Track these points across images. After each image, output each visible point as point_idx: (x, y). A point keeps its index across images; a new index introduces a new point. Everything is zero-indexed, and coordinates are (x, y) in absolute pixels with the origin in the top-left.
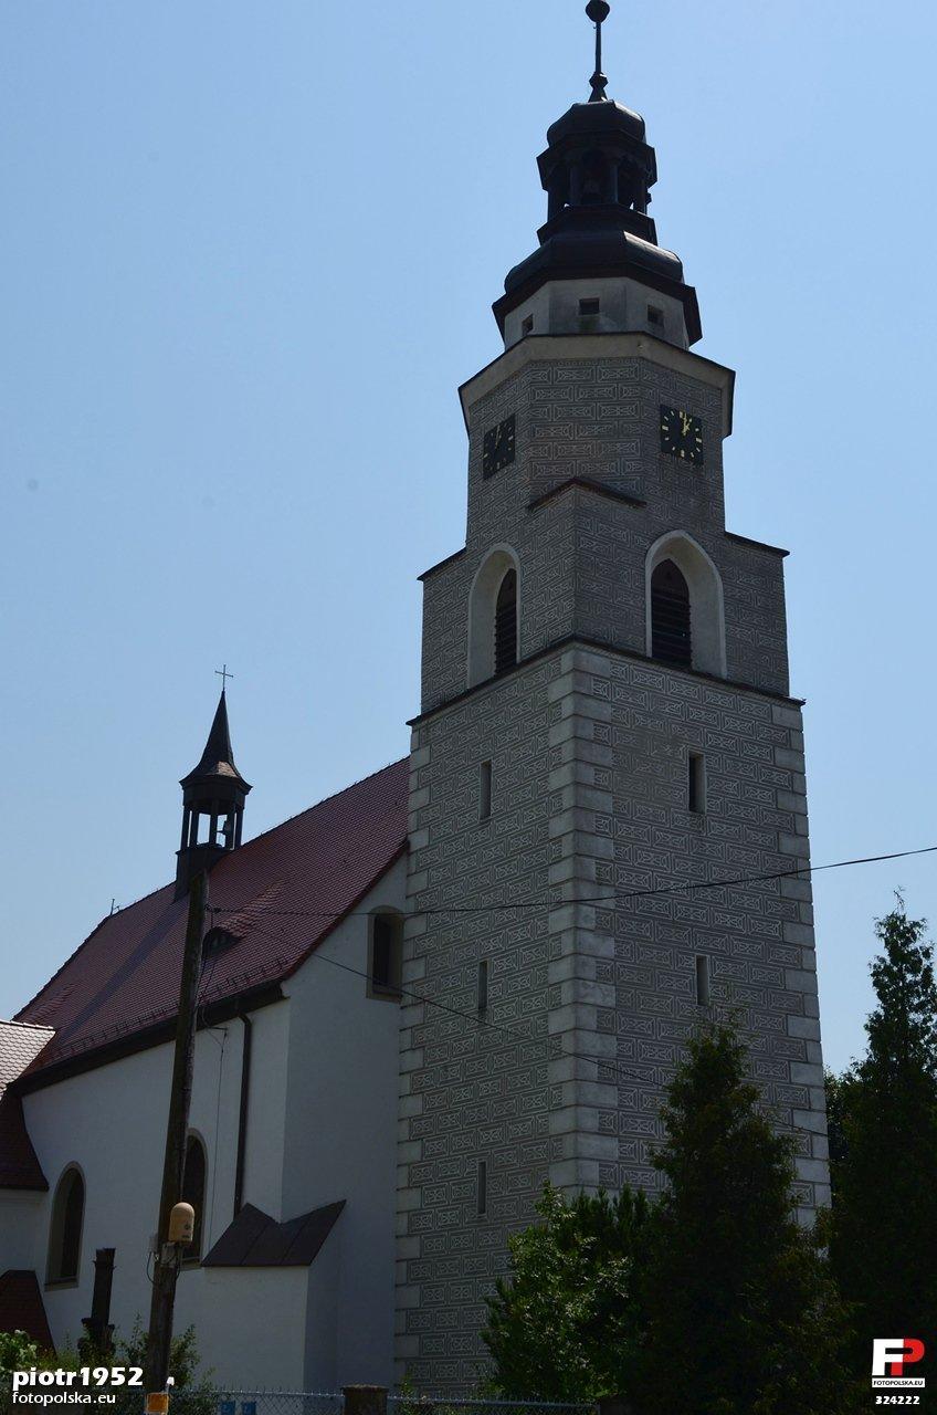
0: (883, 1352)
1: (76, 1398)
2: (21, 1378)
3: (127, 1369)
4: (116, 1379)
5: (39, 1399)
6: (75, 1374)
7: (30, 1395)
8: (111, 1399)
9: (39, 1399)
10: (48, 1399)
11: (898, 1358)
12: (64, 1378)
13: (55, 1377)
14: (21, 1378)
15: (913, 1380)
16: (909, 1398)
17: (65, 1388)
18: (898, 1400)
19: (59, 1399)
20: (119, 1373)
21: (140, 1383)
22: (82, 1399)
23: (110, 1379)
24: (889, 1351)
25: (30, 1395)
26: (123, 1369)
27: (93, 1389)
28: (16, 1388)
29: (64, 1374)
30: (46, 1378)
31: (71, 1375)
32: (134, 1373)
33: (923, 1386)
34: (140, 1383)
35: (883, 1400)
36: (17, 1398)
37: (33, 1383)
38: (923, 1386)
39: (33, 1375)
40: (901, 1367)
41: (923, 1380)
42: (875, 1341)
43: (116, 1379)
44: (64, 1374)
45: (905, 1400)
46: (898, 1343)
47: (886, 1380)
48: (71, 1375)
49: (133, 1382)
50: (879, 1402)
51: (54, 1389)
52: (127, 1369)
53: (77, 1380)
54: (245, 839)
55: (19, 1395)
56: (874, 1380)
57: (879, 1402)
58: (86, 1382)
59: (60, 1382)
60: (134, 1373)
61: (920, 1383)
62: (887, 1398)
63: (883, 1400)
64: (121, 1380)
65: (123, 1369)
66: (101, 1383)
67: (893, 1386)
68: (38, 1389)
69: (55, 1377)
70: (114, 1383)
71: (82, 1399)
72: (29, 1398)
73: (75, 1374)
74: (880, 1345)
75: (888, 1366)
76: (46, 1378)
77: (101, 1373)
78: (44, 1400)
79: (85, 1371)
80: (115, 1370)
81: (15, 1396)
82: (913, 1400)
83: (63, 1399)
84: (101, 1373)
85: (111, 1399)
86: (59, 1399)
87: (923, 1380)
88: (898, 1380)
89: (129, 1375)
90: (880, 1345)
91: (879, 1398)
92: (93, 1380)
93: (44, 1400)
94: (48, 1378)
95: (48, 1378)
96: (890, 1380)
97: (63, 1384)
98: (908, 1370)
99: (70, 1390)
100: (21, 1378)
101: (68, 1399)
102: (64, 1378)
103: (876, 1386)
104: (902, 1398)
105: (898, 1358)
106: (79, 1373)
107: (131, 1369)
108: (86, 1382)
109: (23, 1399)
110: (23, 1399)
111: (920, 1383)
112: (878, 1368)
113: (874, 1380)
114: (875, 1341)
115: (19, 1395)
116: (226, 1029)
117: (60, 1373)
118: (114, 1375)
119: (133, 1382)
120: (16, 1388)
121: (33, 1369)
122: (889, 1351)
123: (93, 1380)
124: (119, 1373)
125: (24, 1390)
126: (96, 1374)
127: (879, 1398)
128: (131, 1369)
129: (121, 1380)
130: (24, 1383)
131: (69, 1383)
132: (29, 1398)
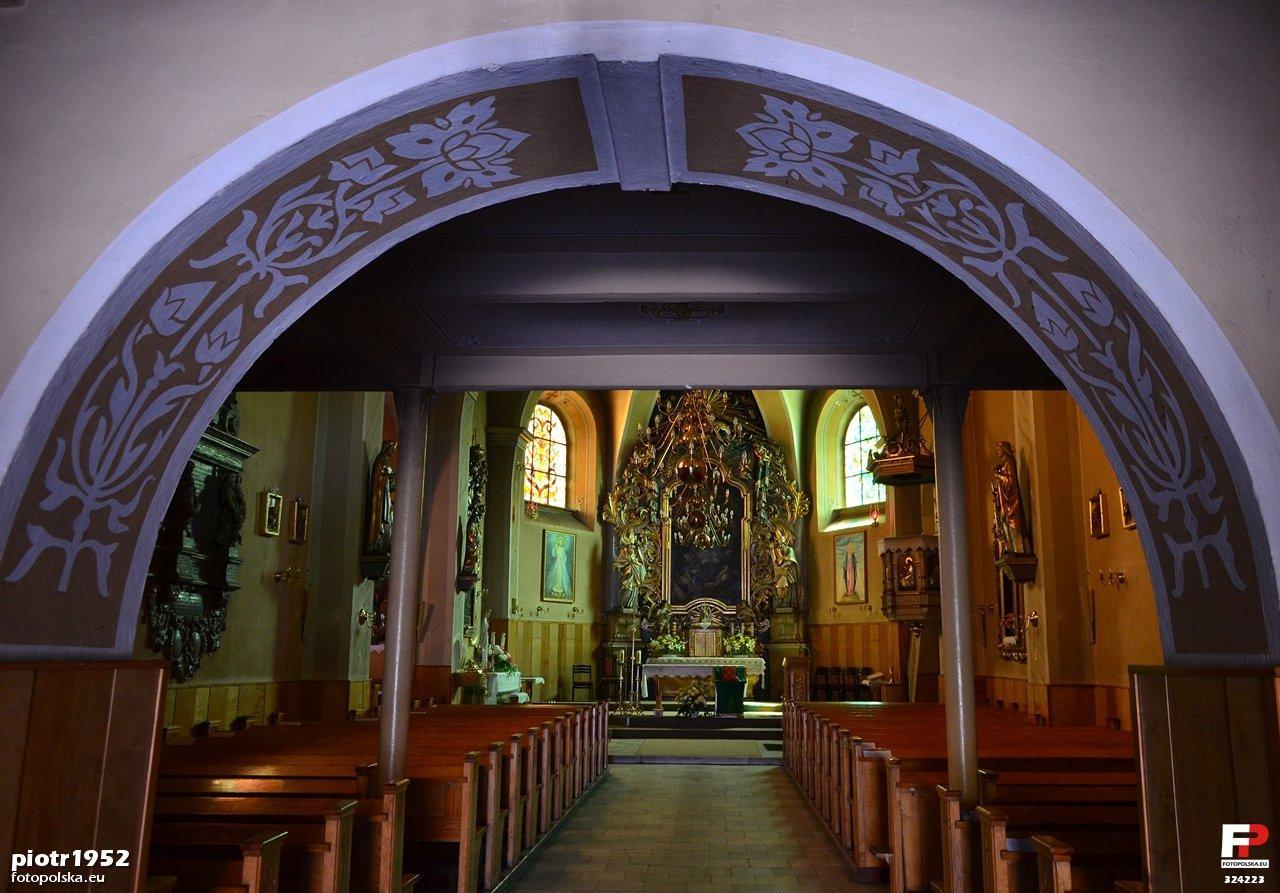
0: (1231, 836)
1: (70, 878)
2: (19, 860)
3: (115, 852)
4: (105, 860)
5: (35, 879)
6: (68, 856)
7: (28, 875)
8: (100, 878)
9: (35, 879)
10: (44, 878)
11: (1245, 842)
12: (58, 860)
13: (50, 859)
14: (18, 861)
15: (1259, 861)
16: (1255, 878)
17: (59, 868)
18: (1245, 879)
19: (53, 878)
20: (108, 855)
21: (127, 864)
22: (74, 878)
23: (99, 860)
24: (1237, 835)
25: (28, 875)
26: (111, 852)
27: (84, 869)
28: (14, 869)
29: (58, 856)
30: (42, 860)
31: (64, 857)
32: (121, 855)
33: (1267, 867)
34: (127, 864)
35: (1231, 879)
36: (16, 878)
37: (30, 864)
38: (1267, 867)
39: (30, 857)
40: (1247, 849)
41: (1268, 861)
42: (1224, 826)
43: (105, 860)
44: (58, 856)
45: (1251, 879)
46: (1245, 828)
47: (1234, 861)
48: (64, 857)
49: (120, 863)
50: (1227, 881)
51: (49, 870)
52: (115, 852)
53: (71, 860)
54: (121, 378)
55: (17, 875)
56: (1223, 861)
57: (1227, 881)
58: (78, 863)
59: (54, 863)
60: (121, 855)
61: (1265, 864)
62: (1235, 878)
63: (1231, 879)
64: (110, 861)
65: (111, 852)
66: (91, 864)
67: (1240, 867)
68: (35, 870)
69: (50, 859)
70: (103, 864)
71: (74, 878)
72: (26, 878)
73: (68, 856)
74: (1228, 830)
75: (1236, 849)
76: (42, 860)
77: (91, 855)
78: (40, 879)
79: (77, 853)
80: (104, 853)
81: (13, 876)
82: (1251, 879)
83: (58, 879)
84: (91, 855)
85: (100, 878)
86: (53, 878)
87: (1268, 861)
88: (1245, 861)
89: (116, 857)
90: (1228, 830)
91: (1228, 878)
92: (84, 861)
93: (40, 879)
94: (42, 860)
95: (42, 860)
96: (1237, 861)
97: (57, 865)
98: (1253, 852)
99: (64, 870)
100: (19, 860)
101: (61, 879)
102: (58, 860)
103: (1225, 867)
104: (1248, 878)
105: (1245, 842)
106: (71, 855)
107: (119, 852)
108: (78, 863)
109: (21, 879)
110: (21, 879)
111: (1265, 864)
112: (1227, 851)
113: (1223, 861)
114: (1224, 826)
115: (17, 875)
116: (869, 195)
117: (54, 855)
118: (103, 857)
119: (120, 863)
120: (14, 869)
121: (30, 851)
122: (1237, 835)
123: (84, 861)
124: (108, 855)
125: (22, 870)
126: (87, 856)
127: (1228, 878)
128: (119, 852)
129: (110, 861)
130: (22, 864)
131: (63, 864)
132: (26, 878)
